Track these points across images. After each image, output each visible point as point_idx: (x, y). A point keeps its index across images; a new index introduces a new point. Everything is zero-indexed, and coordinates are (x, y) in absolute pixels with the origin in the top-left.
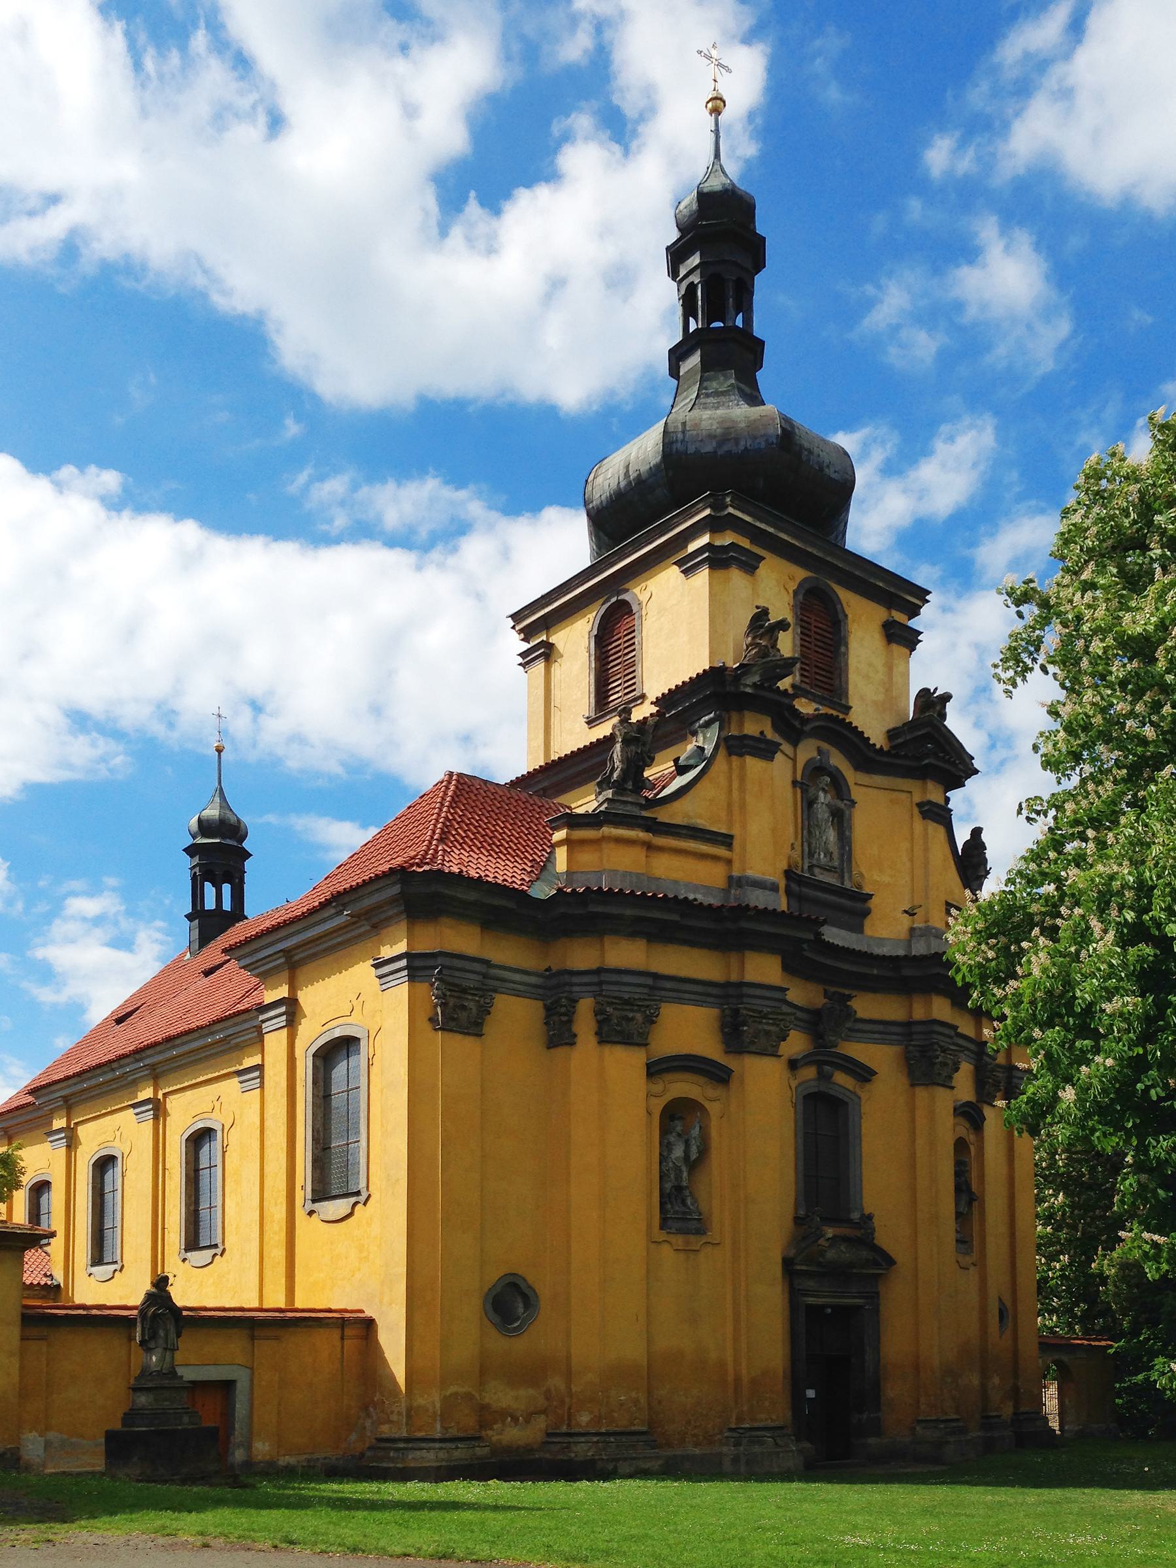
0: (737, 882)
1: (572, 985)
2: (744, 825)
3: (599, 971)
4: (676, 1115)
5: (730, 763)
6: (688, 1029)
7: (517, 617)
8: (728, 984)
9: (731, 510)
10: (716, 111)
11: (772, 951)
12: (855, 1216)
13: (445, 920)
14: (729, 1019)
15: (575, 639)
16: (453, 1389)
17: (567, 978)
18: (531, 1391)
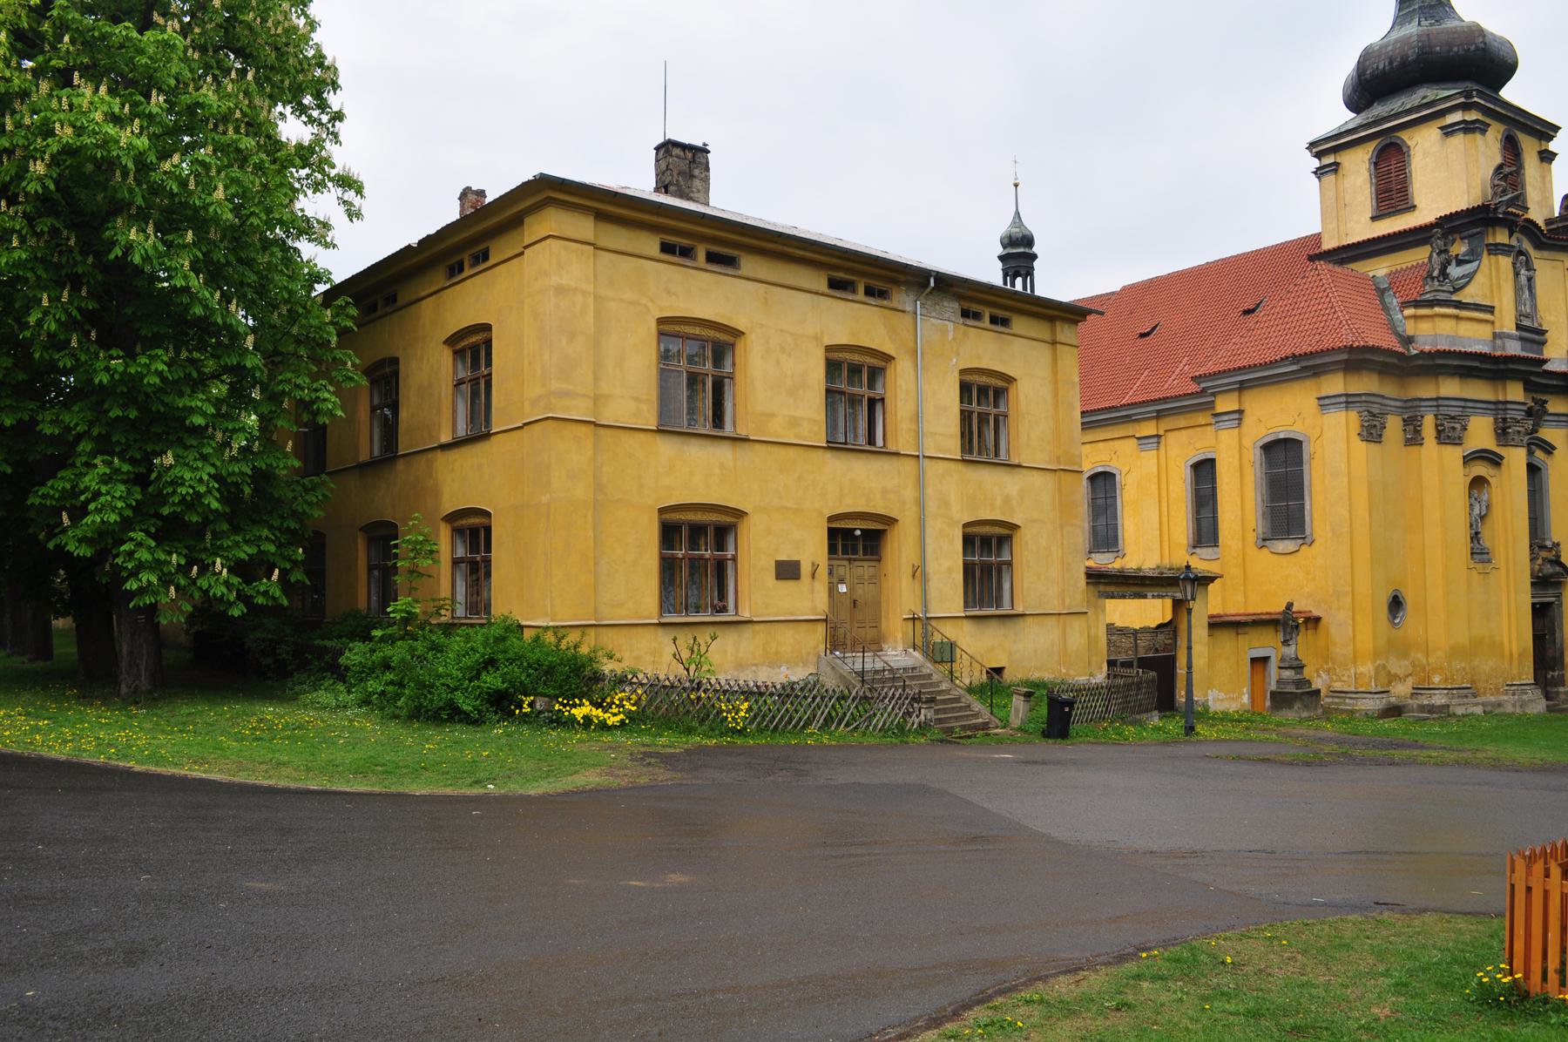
2: (1500, 300)
3: (1437, 399)
4: (1478, 483)
6: (1480, 432)
7: (1312, 145)
8: (1498, 402)
11: (1519, 379)
12: (1549, 544)
15: (1358, 164)
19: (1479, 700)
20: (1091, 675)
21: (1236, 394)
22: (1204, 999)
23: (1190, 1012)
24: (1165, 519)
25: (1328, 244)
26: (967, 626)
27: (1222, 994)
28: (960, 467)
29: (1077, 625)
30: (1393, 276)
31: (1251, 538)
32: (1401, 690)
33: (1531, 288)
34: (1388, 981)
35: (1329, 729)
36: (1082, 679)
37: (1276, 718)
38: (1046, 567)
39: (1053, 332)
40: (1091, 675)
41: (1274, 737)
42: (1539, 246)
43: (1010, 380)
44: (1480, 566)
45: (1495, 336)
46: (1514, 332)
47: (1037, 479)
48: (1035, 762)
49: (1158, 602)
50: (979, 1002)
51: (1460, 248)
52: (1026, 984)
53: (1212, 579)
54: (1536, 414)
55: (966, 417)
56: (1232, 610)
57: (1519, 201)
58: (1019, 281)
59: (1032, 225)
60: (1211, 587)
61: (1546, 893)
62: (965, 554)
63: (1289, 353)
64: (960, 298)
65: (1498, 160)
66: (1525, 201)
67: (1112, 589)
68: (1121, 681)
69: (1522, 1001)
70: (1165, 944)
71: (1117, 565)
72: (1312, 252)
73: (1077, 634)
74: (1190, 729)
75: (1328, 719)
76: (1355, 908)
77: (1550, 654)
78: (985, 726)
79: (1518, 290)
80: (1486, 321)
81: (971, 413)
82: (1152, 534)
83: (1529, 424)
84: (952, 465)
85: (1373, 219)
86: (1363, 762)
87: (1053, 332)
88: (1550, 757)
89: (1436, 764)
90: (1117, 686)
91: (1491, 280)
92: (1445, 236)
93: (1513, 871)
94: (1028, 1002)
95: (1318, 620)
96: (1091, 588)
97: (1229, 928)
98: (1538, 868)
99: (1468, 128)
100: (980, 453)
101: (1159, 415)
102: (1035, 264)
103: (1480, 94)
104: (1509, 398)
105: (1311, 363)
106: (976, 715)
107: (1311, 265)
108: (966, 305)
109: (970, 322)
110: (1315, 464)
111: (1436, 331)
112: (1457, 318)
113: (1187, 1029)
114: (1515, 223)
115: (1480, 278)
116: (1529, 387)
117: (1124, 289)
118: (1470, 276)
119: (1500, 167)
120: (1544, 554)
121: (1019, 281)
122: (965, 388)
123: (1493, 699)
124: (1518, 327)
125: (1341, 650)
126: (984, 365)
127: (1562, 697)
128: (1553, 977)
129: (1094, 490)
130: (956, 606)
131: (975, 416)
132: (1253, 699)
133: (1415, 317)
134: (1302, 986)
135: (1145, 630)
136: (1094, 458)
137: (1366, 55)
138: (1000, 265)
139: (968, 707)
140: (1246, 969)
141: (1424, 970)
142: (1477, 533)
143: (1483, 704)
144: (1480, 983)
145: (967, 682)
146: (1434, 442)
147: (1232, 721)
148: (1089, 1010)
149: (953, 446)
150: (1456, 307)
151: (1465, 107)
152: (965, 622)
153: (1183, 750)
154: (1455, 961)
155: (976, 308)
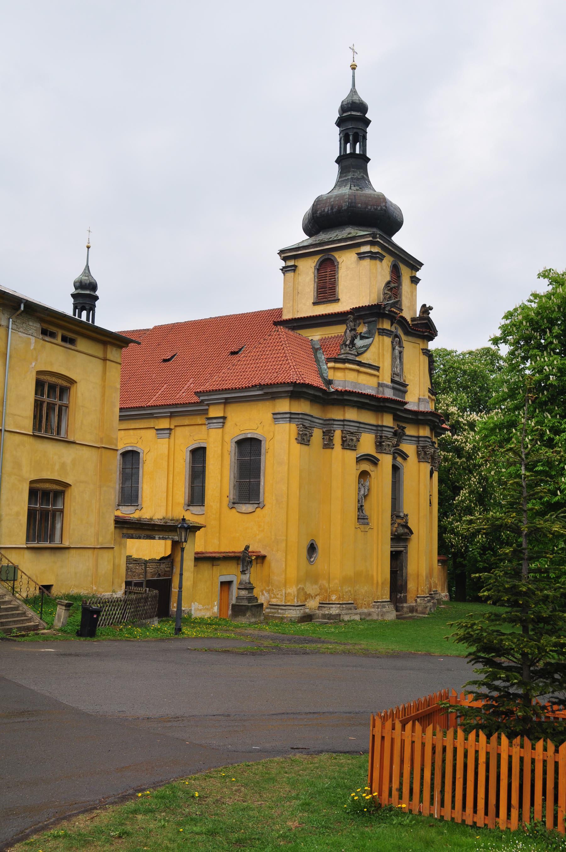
0: (379, 385)
1: (334, 424)
2: (383, 362)
3: (344, 421)
4: (364, 475)
5: (379, 338)
6: (367, 444)
7: (281, 252)
8: (377, 426)
9: (378, 240)
10: (354, 69)
11: (390, 413)
12: (402, 515)
13: (302, 400)
14: (379, 440)
15: (308, 268)
16: (300, 586)
17: (332, 422)
18: (316, 587)
19: (358, 611)
20: (114, 591)
21: (222, 406)
22: (179, 824)
23: (170, 835)
24: (171, 486)
25: (286, 316)
26: (28, 555)
27: (192, 820)
28: (31, 440)
29: (106, 556)
30: (323, 341)
31: (226, 501)
32: (313, 604)
33: (401, 358)
34: (298, 802)
35: (268, 630)
36: (107, 594)
37: (235, 623)
38: (87, 515)
39: (105, 352)
40: (114, 591)
41: (233, 635)
42: (407, 333)
43: (72, 382)
44: (362, 527)
45: (379, 385)
46: (389, 383)
47: (86, 452)
48: (70, 655)
49: (162, 542)
50: (18, 841)
51: (363, 329)
52: (54, 824)
53: (199, 528)
54: (399, 435)
55: (38, 405)
56: (211, 549)
57: (398, 304)
58: (84, 313)
59: (97, 276)
60: (198, 533)
61: (393, 740)
62: (30, 502)
63: (257, 382)
64: (41, 320)
65: (388, 278)
66: (401, 305)
67: (131, 532)
68: (134, 597)
69: (377, 810)
70: (155, 785)
71: (136, 515)
72: (276, 320)
73: (106, 563)
74: (178, 630)
75: (267, 624)
76: (279, 752)
77: (399, 583)
78: (36, 628)
79: (393, 358)
80: (375, 375)
81: (42, 403)
82: (160, 497)
83: (395, 441)
84: (25, 438)
85: (314, 304)
86: (287, 652)
87: (105, 352)
88: (397, 648)
89: (331, 653)
90: (131, 600)
91: (378, 350)
92: (355, 320)
93: (374, 727)
94: (56, 837)
95: (264, 557)
96: (118, 530)
97: (200, 771)
98: (389, 724)
99: (373, 256)
100: (46, 431)
101: (172, 415)
102: (97, 303)
103: (381, 237)
104: (385, 424)
105: (270, 390)
106: (30, 620)
107: (275, 328)
108: (45, 326)
109: (47, 339)
110: (268, 456)
111: (344, 379)
112: (358, 371)
113: (167, 848)
114: (395, 318)
115: (372, 349)
116: (396, 418)
117: (155, 328)
118: (368, 347)
119: (388, 283)
120: (399, 521)
121: (84, 313)
122: (39, 384)
123: (366, 611)
124: (393, 381)
125: (277, 578)
126: (55, 369)
127: (405, 609)
128: (395, 793)
129: (124, 462)
130: (20, 540)
131: (45, 405)
132: (220, 609)
133: (334, 368)
134: (243, 810)
135: (152, 561)
136: (126, 440)
137: (318, 202)
138: (72, 300)
139: (24, 614)
140: (208, 799)
141: (320, 793)
142: (362, 506)
143: (360, 614)
144: (353, 800)
145: (24, 595)
146: (340, 447)
147: (206, 624)
148: (99, 839)
149: (27, 425)
150: (358, 365)
151: (372, 243)
152: (27, 552)
153: (173, 645)
154: (338, 785)
155: (53, 329)
